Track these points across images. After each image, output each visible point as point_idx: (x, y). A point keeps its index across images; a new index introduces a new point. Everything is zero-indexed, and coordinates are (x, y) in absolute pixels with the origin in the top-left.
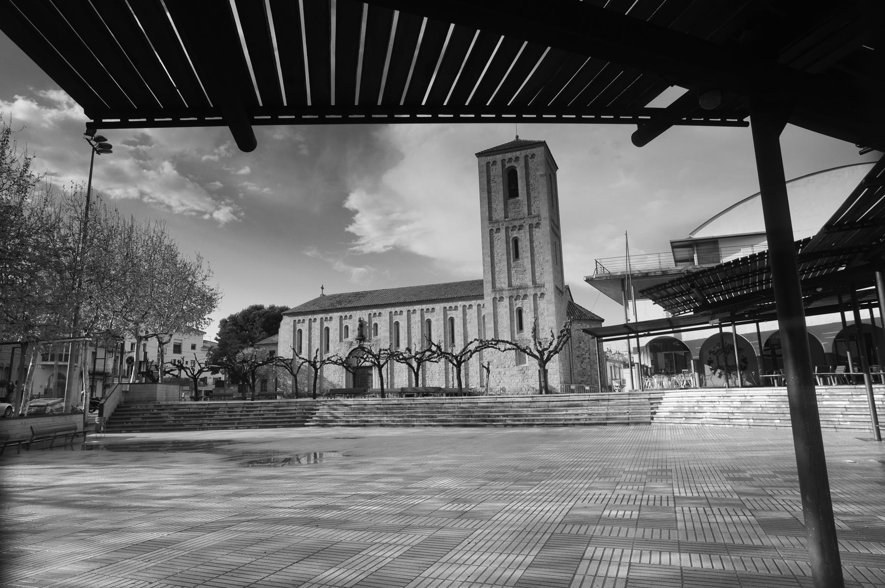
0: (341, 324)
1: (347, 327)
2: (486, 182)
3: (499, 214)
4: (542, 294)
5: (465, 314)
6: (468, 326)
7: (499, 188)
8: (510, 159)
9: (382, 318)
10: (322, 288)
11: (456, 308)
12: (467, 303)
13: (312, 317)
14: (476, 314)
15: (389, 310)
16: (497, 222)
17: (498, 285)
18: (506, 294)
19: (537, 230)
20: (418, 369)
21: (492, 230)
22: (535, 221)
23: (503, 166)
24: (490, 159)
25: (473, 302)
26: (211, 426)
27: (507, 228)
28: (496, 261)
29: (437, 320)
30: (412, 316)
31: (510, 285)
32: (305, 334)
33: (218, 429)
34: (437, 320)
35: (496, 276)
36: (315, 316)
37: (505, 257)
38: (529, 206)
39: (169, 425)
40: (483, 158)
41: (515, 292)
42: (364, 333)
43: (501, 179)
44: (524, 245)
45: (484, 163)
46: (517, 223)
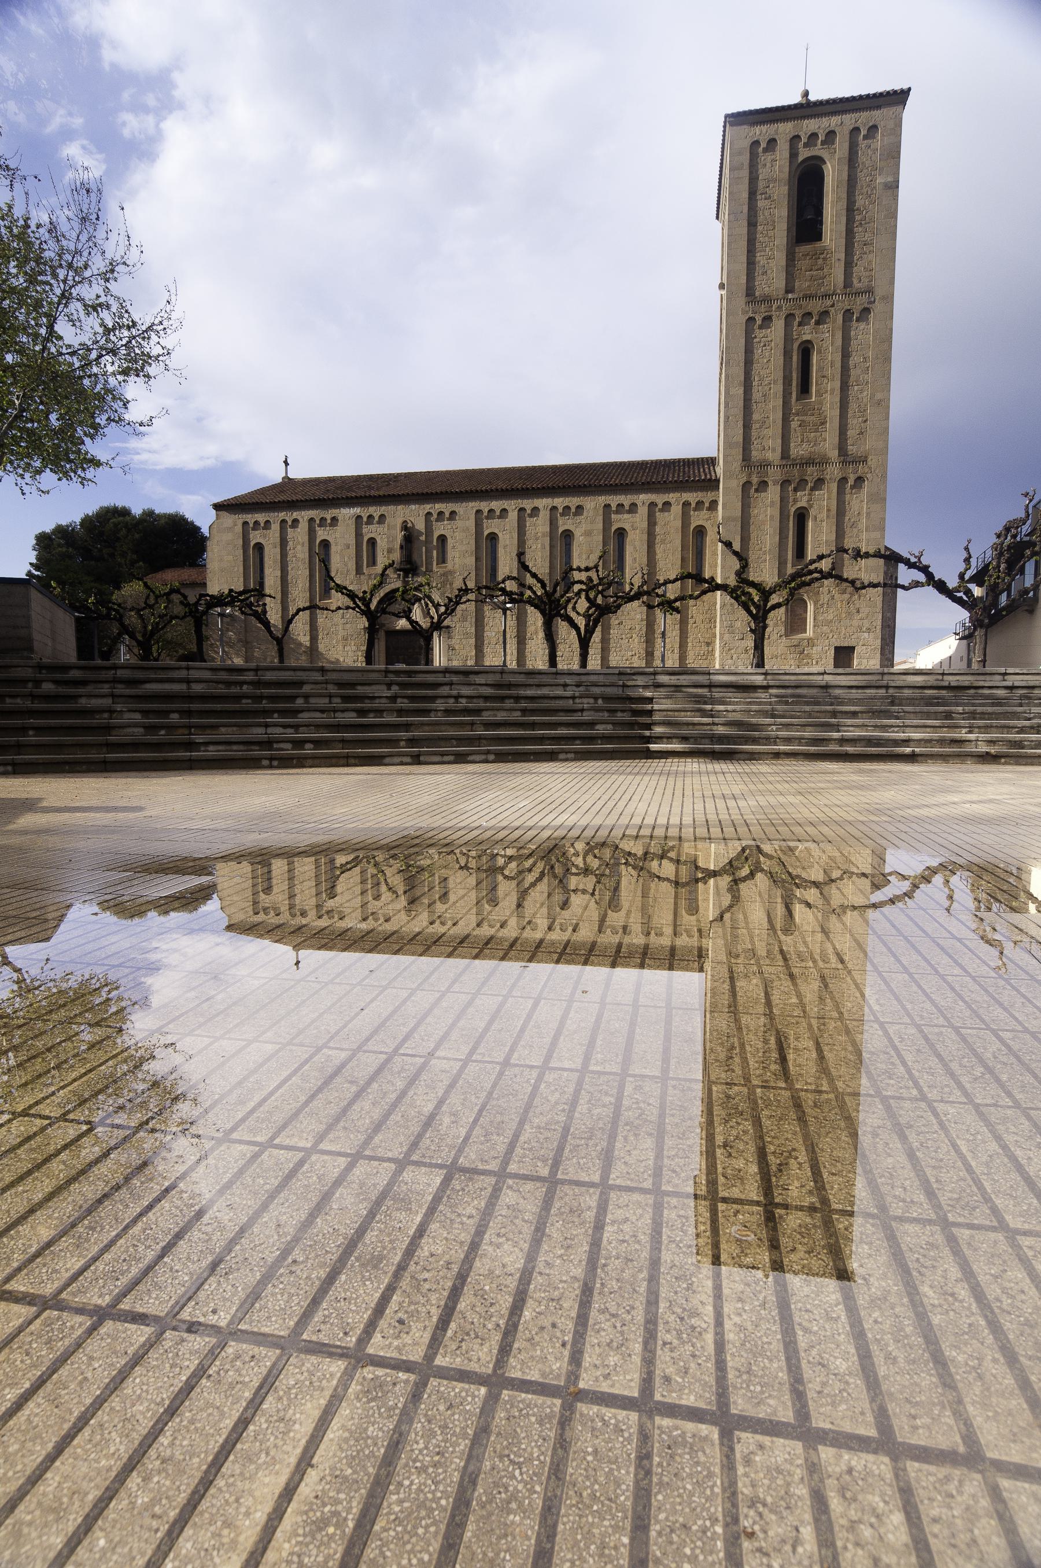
0: (359, 535)
1: (372, 542)
2: (745, 195)
3: (772, 278)
4: (860, 480)
5: (652, 523)
6: (659, 550)
7: (777, 213)
8: (814, 136)
9: (459, 523)
10: (286, 463)
11: (633, 508)
12: (659, 499)
13: (289, 516)
14: (679, 523)
15: (473, 506)
16: (767, 299)
17: (756, 455)
18: (774, 475)
19: (862, 325)
20: (590, 631)
21: (751, 320)
22: (861, 301)
23: (793, 154)
24: (762, 132)
25: (672, 497)
26: (309, 750)
27: (790, 317)
28: (756, 395)
29: (588, 533)
30: (529, 521)
31: (785, 455)
32: (272, 555)
33: (347, 761)
34: (588, 533)
35: (754, 434)
36: (296, 515)
37: (780, 387)
38: (849, 265)
39: (135, 746)
40: (745, 129)
41: (796, 472)
42: (415, 557)
43: (785, 189)
44: (825, 362)
45: (746, 144)
46: (816, 306)
